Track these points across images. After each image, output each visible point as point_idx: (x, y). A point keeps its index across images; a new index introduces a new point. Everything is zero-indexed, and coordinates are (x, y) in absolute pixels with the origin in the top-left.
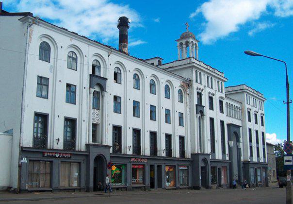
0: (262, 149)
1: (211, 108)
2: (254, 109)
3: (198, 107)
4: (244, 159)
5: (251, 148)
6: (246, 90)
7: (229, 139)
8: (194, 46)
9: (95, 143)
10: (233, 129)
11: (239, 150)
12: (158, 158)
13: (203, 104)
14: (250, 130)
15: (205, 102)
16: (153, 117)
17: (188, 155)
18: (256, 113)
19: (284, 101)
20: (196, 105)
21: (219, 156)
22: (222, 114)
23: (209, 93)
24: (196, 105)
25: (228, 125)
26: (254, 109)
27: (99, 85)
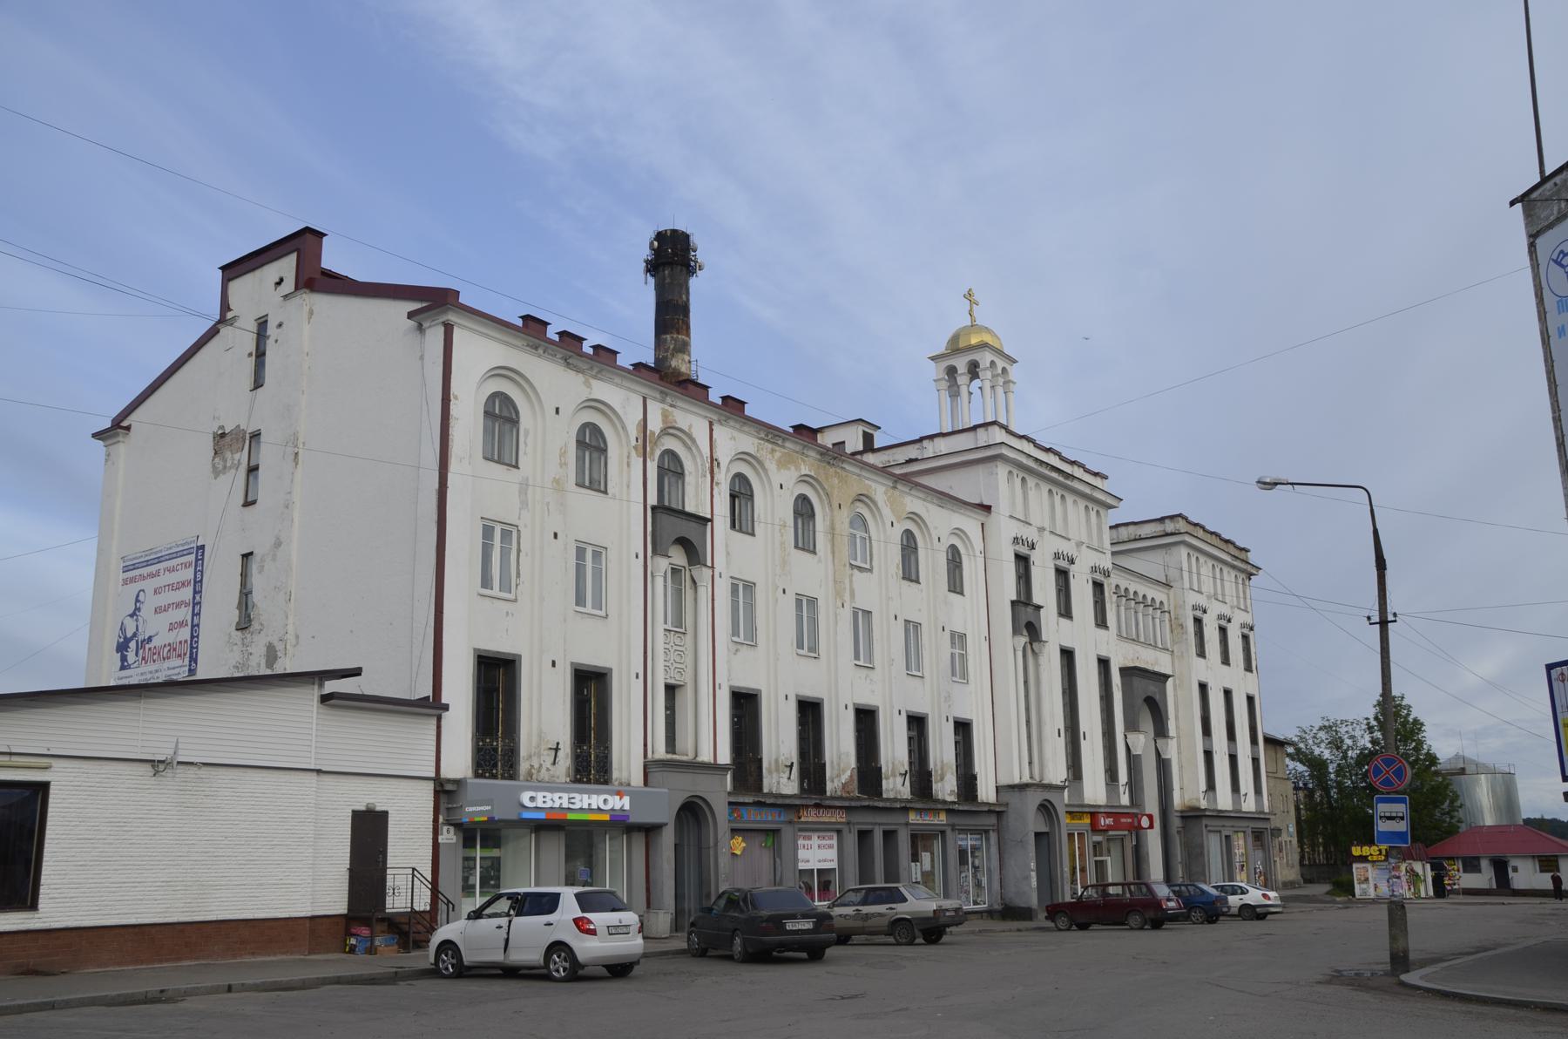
0: (1250, 762)
1: (1065, 611)
2: (1215, 609)
3: (1022, 608)
4: (1182, 796)
5: (1208, 755)
6: (1188, 538)
7: (1131, 726)
8: (1001, 380)
9: (674, 757)
10: (1144, 687)
11: (1163, 766)
12: (888, 805)
13: (1037, 598)
14: (1203, 687)
15: (1044, 590)
16: (807, 641)
17: (986, 792)
18: (1223, 623)
19: (1369, 618)
20: (1013, 603)
21: (1094, 790)
22: (1102, 632)
23: (1057, 556)
24: (1013, 603)
25: (1126, 672)
26: (1215, 609)
27: (684, 543)
